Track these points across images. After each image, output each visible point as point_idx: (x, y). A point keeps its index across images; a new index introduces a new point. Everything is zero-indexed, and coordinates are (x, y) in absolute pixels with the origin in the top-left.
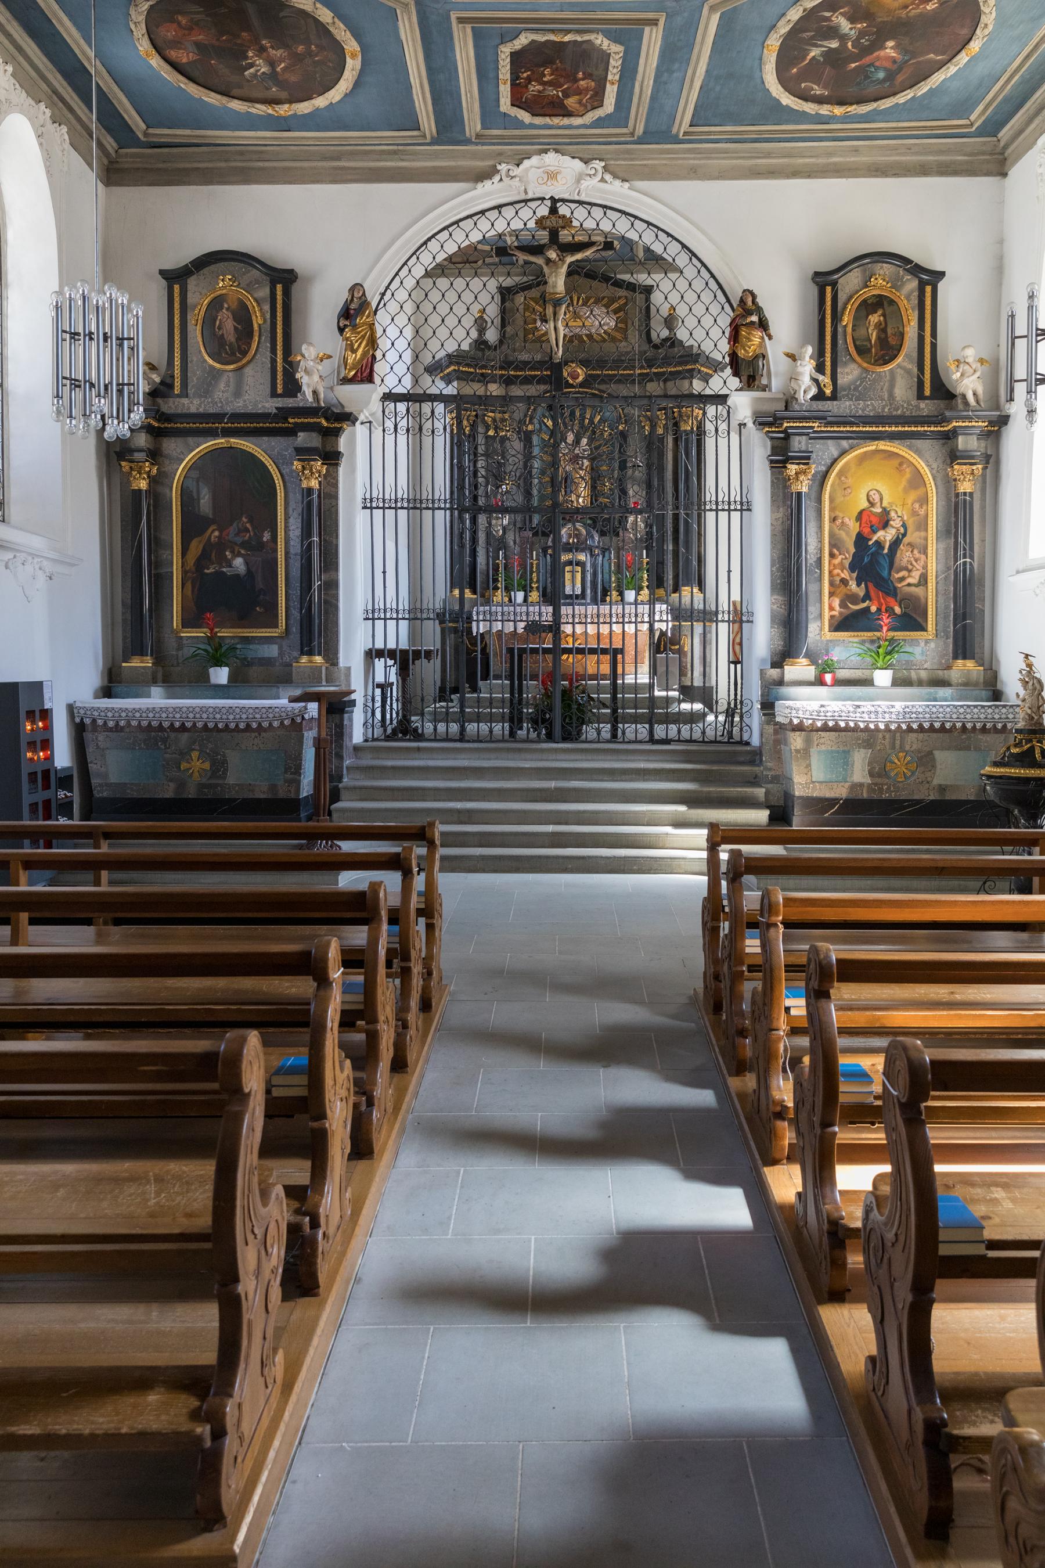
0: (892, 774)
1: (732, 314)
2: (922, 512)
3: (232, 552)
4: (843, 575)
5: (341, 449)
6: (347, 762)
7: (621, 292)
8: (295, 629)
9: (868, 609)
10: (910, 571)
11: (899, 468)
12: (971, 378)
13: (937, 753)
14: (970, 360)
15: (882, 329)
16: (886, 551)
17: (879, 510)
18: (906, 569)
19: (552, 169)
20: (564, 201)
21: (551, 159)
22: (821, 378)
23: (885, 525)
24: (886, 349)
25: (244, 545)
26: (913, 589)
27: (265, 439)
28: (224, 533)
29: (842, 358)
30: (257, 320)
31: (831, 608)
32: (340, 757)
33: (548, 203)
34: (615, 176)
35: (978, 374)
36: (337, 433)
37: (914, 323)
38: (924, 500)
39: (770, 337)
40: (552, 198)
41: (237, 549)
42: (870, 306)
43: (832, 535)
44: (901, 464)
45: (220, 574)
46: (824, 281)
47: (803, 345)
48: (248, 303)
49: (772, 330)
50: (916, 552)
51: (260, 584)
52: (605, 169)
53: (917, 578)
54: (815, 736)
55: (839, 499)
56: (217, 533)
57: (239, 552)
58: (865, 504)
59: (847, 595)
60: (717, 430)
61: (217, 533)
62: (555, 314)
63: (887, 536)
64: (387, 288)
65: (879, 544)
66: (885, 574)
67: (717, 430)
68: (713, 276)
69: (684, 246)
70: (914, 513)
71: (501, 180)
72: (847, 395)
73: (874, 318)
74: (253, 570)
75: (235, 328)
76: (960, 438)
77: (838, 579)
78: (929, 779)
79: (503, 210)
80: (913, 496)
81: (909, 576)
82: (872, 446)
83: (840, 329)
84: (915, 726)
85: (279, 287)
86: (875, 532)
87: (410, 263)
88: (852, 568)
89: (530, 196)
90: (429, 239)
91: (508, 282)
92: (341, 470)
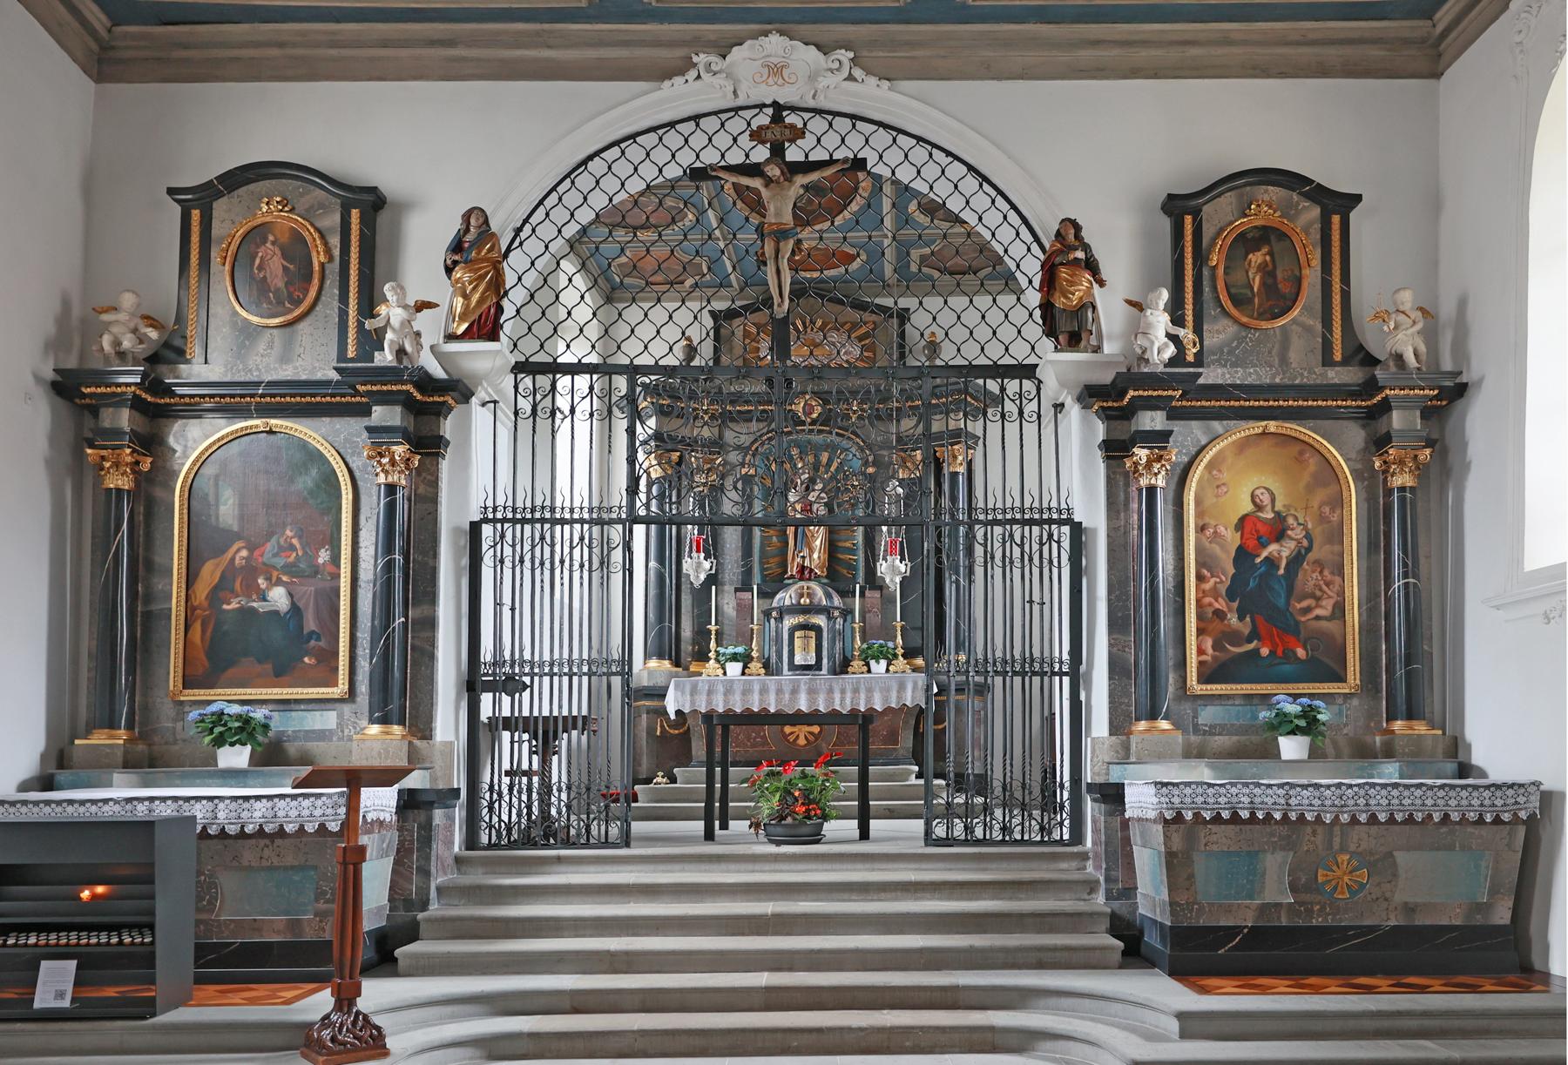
0: (1328, 889)
1: (1042, 257)
2: (1335, 518)
3: (268, 579)
4: (1217, 606)
5: (447, 436)
6: (437, 880)
7: (867, 316)
8: (363, 688)
9: (1256, 651)
10: (1318, 599)
11: (1299, 459)
12: (1410, 331)
13: (1400, 856)
14: (1407, 307)
15: (1268, 272)
16: (1281, 571)
17: (1270, 515)
18: (1313, 596)
19: (775, 60)
20: (794, 109)
21: (775, 43)
22: (1181, 332)
23: (1279, 534)
24: (1278, 300)
25: (290, 569)
26: (1324, 624)
27: (326, 420)
28: (256, 553)
29: (1210, 310)
30: (318, 258)
31: (1200, 651)
32: (425, 873)
33: (770, 111)
34: (869, 72)
35: (1419, 326)
36: (441, 411)
37: (1316, 262)
38: (1338, 502)
39: (1101, 283)
40: (775, 104)
41: (275, 574)
42: (1247, 242)
43: (1199, 550)
44: (1301, 453)
45: (247, 613)
46: (1179, 207)
47: (1153, 286)
48: (306, 234)
49: (1105, 273)
50: (1326, 573)
51: (310, 624)
52: (854, 61)
53: (1330, 608)
54: (1202, 832)
55: (1209, 500)
56: (244, 553)
57: (279, 579)
58: (1247, 507)
59: (1223, 632)
60: (1021, 413)
61: (244, 553)
62: (777, 251)
63: (1282, 551)
64: (526, 221)
65: (1271, 562)
66: (1281, 602)
67: (1021, 413)
68: (1014, 207)
69: (971, 168)
70: (1322, 519)
71: (699, 77)
72: (1218, 360)
73: (1257, 258)
74: (301, 605)
75: (285, 268)
76: (1395, 414)
77: (1210, 610)
78: (1388, 895)
79: (703, 121)
80: (1321, 495)
81: (1318, 606)
82: (1257, 427)
83: (1206, 272)
84: (1226, 815)
85: (355, 213)
86: (1264, 546)
87: (561, 189)
88: (1231, 594)
89: (740, 102)
90: (591, 158)
91: (720, 305)
92: (445, 466)
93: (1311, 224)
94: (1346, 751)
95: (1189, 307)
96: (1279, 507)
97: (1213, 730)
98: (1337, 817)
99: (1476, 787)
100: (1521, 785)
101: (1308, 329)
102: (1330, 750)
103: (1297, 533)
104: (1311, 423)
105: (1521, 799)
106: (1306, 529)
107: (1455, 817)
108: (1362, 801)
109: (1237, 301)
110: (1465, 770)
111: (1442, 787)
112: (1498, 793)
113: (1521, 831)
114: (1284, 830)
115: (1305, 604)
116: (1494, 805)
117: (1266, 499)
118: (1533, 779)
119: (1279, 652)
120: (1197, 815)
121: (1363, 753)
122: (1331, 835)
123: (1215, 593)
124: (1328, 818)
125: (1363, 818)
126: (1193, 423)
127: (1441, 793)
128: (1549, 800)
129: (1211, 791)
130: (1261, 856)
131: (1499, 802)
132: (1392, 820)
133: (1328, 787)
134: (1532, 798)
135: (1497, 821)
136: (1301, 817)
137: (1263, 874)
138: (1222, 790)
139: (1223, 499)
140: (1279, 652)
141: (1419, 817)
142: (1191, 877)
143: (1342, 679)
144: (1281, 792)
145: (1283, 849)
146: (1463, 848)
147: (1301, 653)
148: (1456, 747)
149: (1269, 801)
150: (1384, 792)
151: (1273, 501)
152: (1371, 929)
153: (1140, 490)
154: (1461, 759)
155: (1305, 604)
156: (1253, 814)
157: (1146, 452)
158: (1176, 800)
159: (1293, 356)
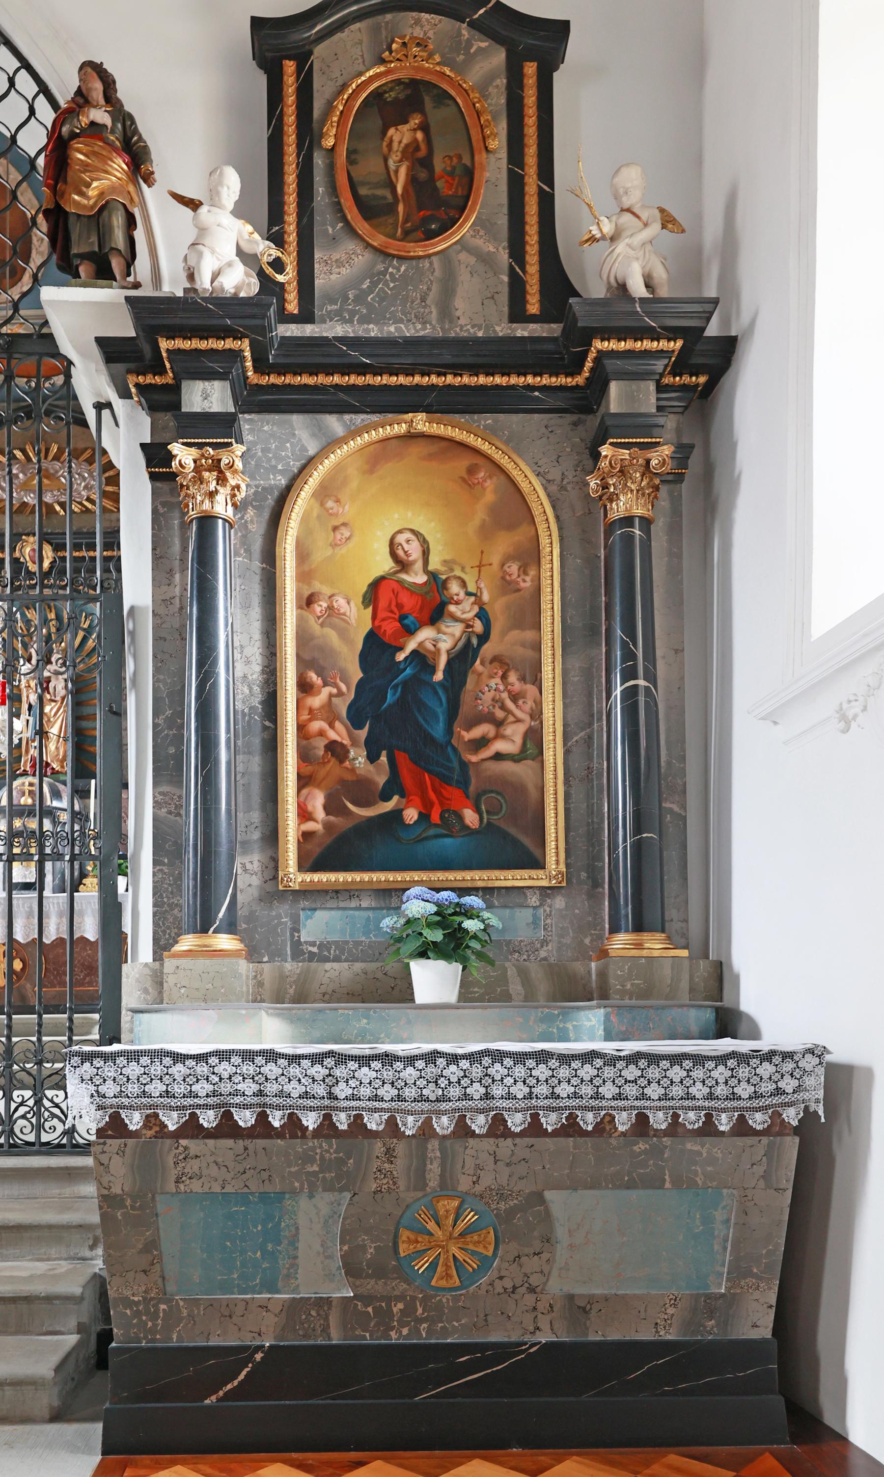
0: (422, 1266)
2: (527, 583)
4: (332, 735)
9: (397, 814)
10: (499, 724)
11: (468, 480)
15: (420, 159)
16: (439, 676)
23: (436, 613)
24: (436, 205)
26: (507, 766)
29: (325, 224)
31: (304, 815)
37: (499, 143)
38: (530, 556)
43: (303, 638)
44: (472, 470)
50: (513, 677)
53: (518, 740)
55: (320, 554)
58: (384, 565)
59: (342, 781)
63: (440, 640)
65: (422, 660)
66: (438, 731)
70: (507, 586)
72: (339, 313)
73: (402, 135)
77: (320, 745)
78: (535, 1280)
80: (503, 544)
81: (498, 736)
83: (319, 161)
84: (208, 1119)
86: (410, 632)
93: (489, 79)
94: (543, 987)
95: (291, 218)
96: (435, 563)
97: (324, 953)
98: (428, 1122)
99: (743, 1058)
100: (788, 1056)
101: (486, 259)
102: (516, 988)
103: (465, 609)
104: (488, 419)
105: (789, 1085)
106: (479, 601)
107: (659, 1120)
108: (476, 1090)
109: (371, 210)
110: (728, 1022)
111: (634, 1058)
112: (743, 1072)
113: (791, 1146)
114: (329, 1148)
115: (477, 732)
116: (734, 1097)
117: (414, 550)
118: (809, 1040)
119: (435, 817)
120: (152, 1120)
121: (572, 990)
122: (423, 1159)
123: (329, 713)
124: (410, 1125)
125: (479, 1123)
126: (296, 419)
127: (632, 1072)
128: (842, 1083)
129: (179, 1070)
130: (288, 1202)
131: (744, 1090)
132: (535, 1128)
133: (410, 1060)
134: (809, 1081)
135: (742, 1128)
136: (357, 1123)
137: (294, 1241)
138: (202, 1069)
139: (343, 551)
140: (435, 817)
141: (588, 1120)
142: (152, 1245)
143: (538, 864)
144: (318, 1071)
145: (329, 1188)
146: (677, 1183)
147: (470, 817)
148: (718, 979)
149: (294, 1088)
150: (520, 1071)
151: (426, 553)
152: (503, 1350)
153: (185, 526)
154: (727, 1002)
155: (477, 732)
156: (262, 1118)
157: (194, 452)
158: (110, 1089)
159: (460, 305)
